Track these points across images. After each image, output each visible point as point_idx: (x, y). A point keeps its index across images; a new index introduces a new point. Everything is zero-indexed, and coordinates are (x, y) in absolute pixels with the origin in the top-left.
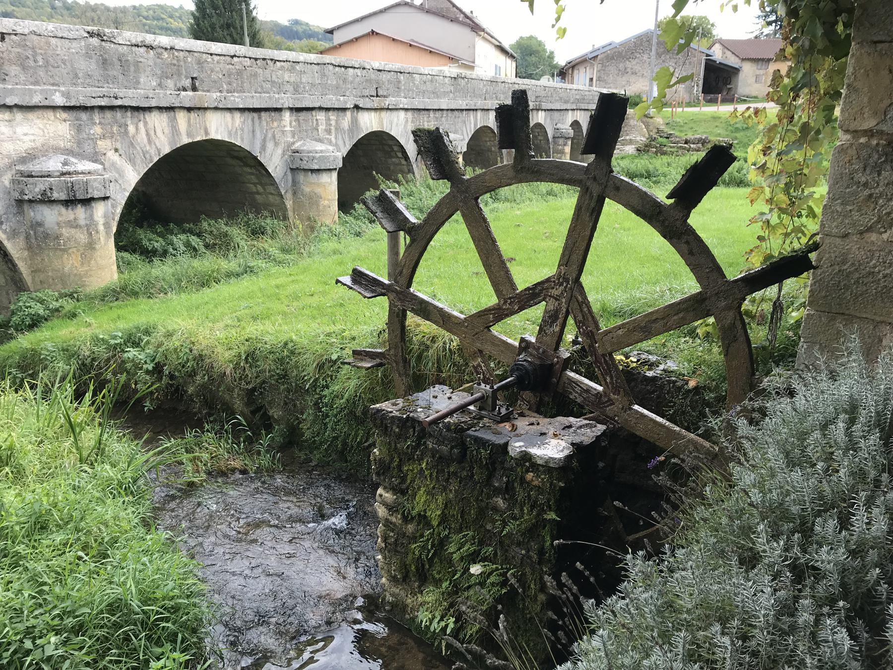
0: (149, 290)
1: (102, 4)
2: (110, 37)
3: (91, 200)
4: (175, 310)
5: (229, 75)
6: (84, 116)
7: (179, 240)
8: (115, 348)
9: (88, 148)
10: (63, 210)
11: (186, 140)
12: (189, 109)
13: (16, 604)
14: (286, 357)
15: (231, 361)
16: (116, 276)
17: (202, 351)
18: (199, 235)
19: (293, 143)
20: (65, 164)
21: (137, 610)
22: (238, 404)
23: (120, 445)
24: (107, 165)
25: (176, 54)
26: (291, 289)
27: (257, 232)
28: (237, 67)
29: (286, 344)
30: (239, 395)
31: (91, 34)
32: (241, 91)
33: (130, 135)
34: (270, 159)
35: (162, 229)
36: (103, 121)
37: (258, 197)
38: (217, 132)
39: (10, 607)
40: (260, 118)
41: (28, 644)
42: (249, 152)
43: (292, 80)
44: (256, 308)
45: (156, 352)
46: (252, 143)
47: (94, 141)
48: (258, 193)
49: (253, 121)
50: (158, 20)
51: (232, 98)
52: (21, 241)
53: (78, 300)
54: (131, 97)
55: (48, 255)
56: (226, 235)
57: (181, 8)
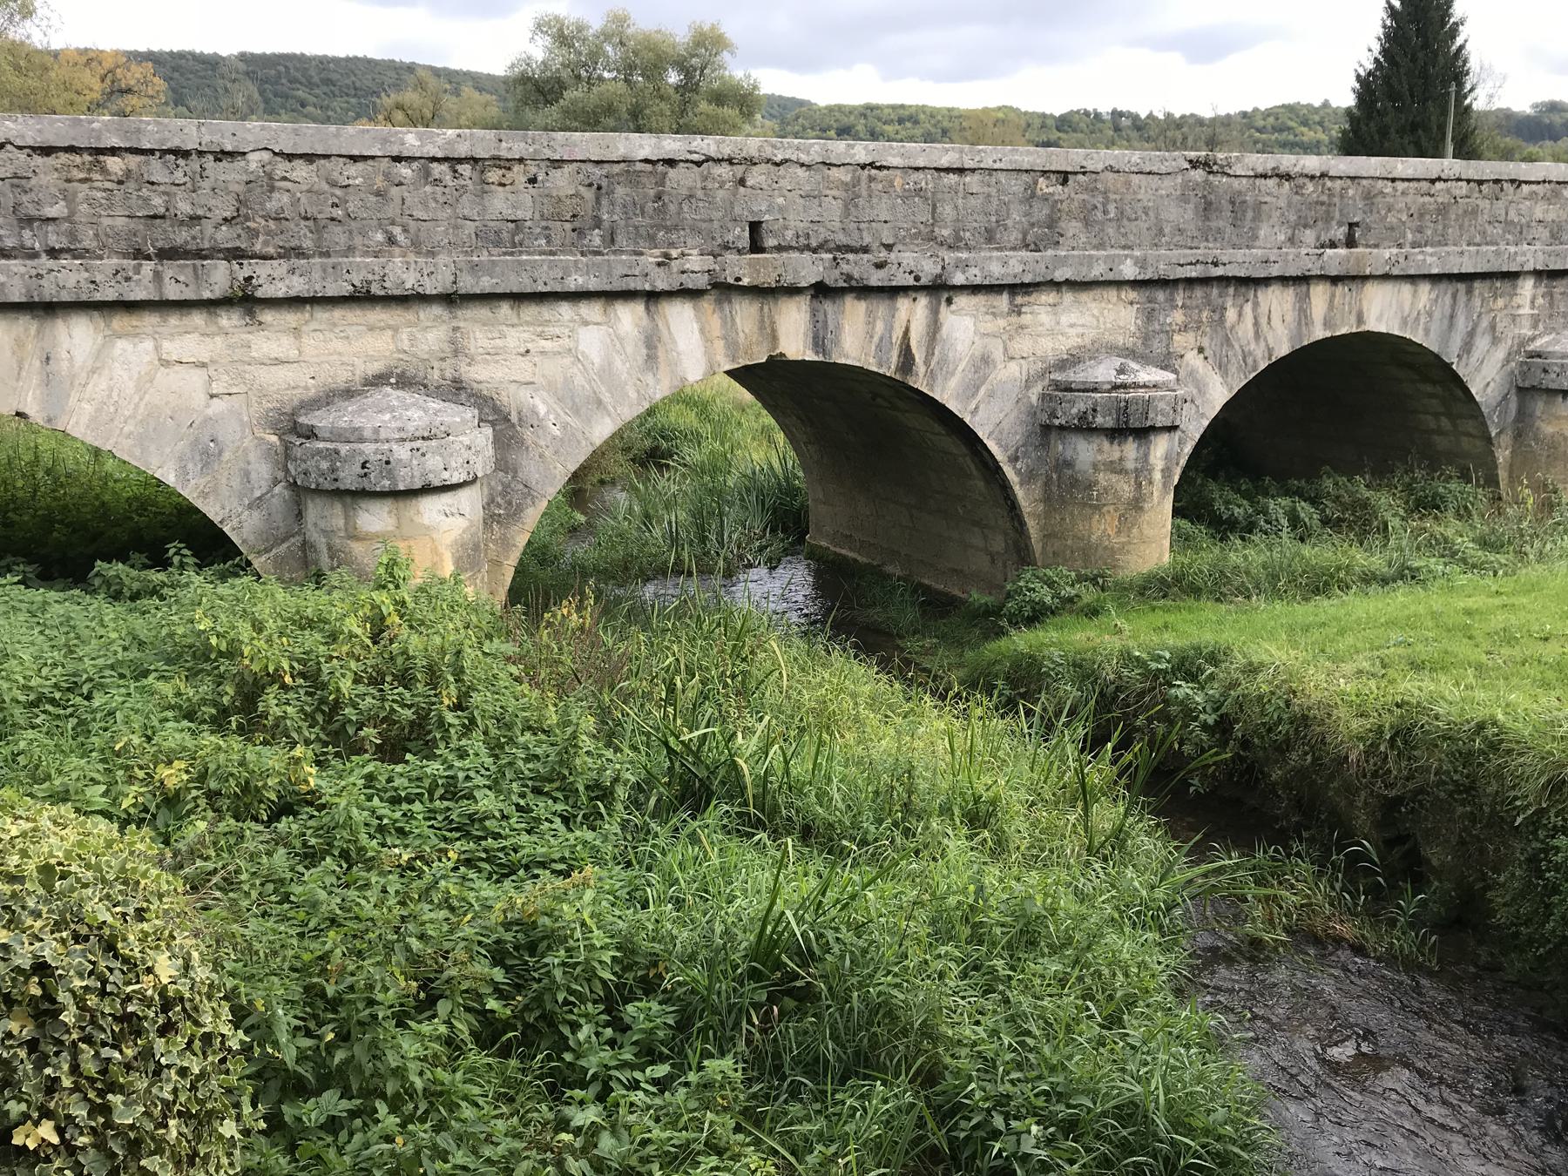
0: (1220, 587)
1: (1192, 115)
2: (1222, 167)
3: (1153, 429)
4: (1264, 627)
5: (1421, 215)
6: (1161, 295)
7: (1278, 506)
8: (1156, 677)
9: (1158, 346)
10: (1106, 444)
11: (1320, 333)
12: (1335, 280)
13: (988, 1049)
14: (1477, 755)
15: (1361, 739)
16: (1167, 558)
17: (1309, 708)
18: (1314, 502)
19: (1533, 339)
20: (1121, 371)
21: (1163, 1134)
22: (1361, 819)
23: (1148, 842)
24: (1182, 373)
25: (1329, 184)
26: (1498, 620)
27: (1427, 505)
28: (1440, 200)
29: (1481, 727)
30: (1366, 803)
31: (1194, 164)
32: (1439, 244)
33: (1228, 325)
34: (1478, 369)
35: (1250, 486)
36: (1188, 302)
37: (1437, 439)
38: (1379, 319)
39: (979, 1052)
40: (1469, 292)
41: (998, 1122)
42: (1437, 357)
43: (1550, 217)
44: (1419, 647)
45: (1225, 695)
46: (1445, 339)
47: (1169, 334)
48: (1440, 432)
49: (1454, 297)
50: (1281, 131)
51: (1420, 257)
52: (1037, 489)
53: (1103, 590)
54: (1238, 261)
55: (1072, 514)
56: (1365, 504)
57: (1326, 104)
